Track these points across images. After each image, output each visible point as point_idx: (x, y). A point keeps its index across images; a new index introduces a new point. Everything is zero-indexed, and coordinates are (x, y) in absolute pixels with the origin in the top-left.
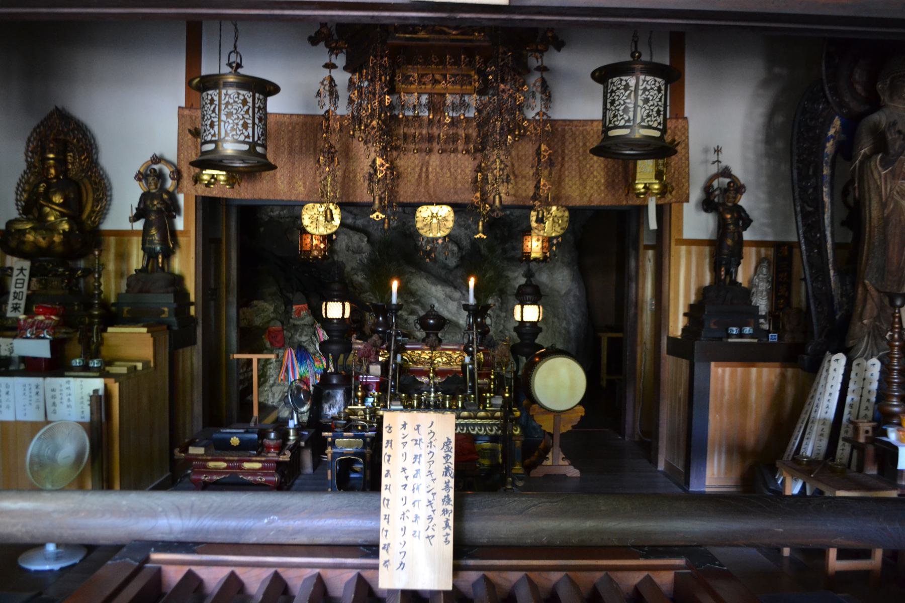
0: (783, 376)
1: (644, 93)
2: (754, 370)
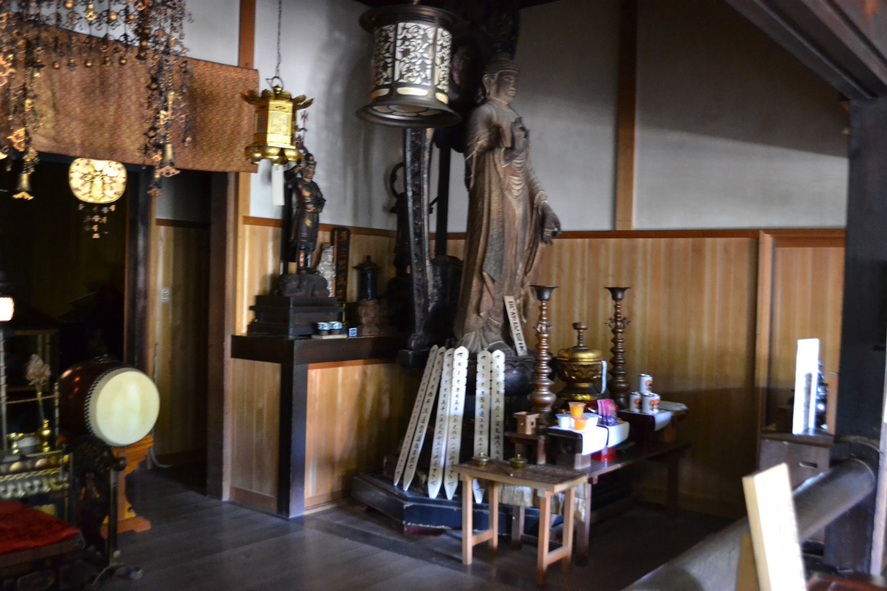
0: (364, 373)
1: (403, 43)
2: (340, 370)
